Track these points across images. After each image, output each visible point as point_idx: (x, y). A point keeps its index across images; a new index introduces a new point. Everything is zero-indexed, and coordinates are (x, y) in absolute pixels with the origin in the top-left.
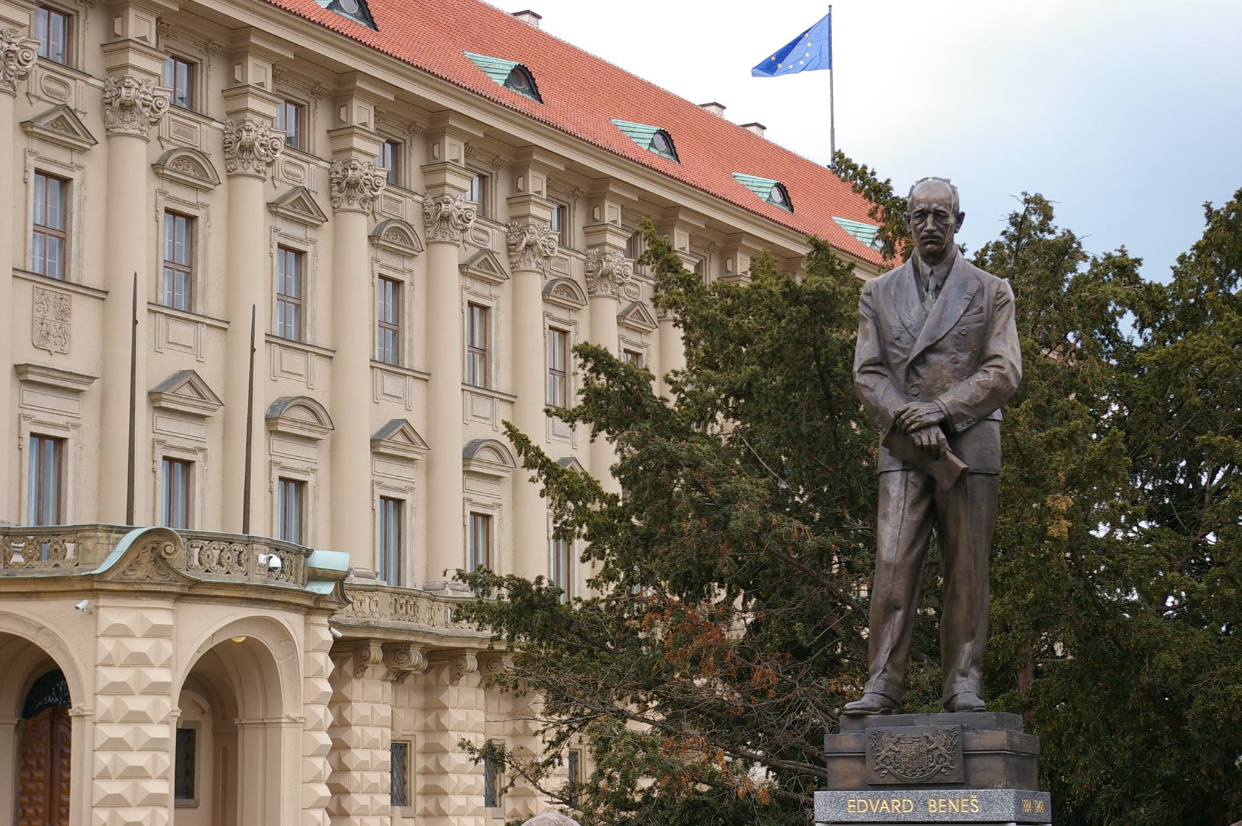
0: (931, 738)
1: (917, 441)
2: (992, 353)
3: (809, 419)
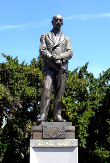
0: (59, 127)
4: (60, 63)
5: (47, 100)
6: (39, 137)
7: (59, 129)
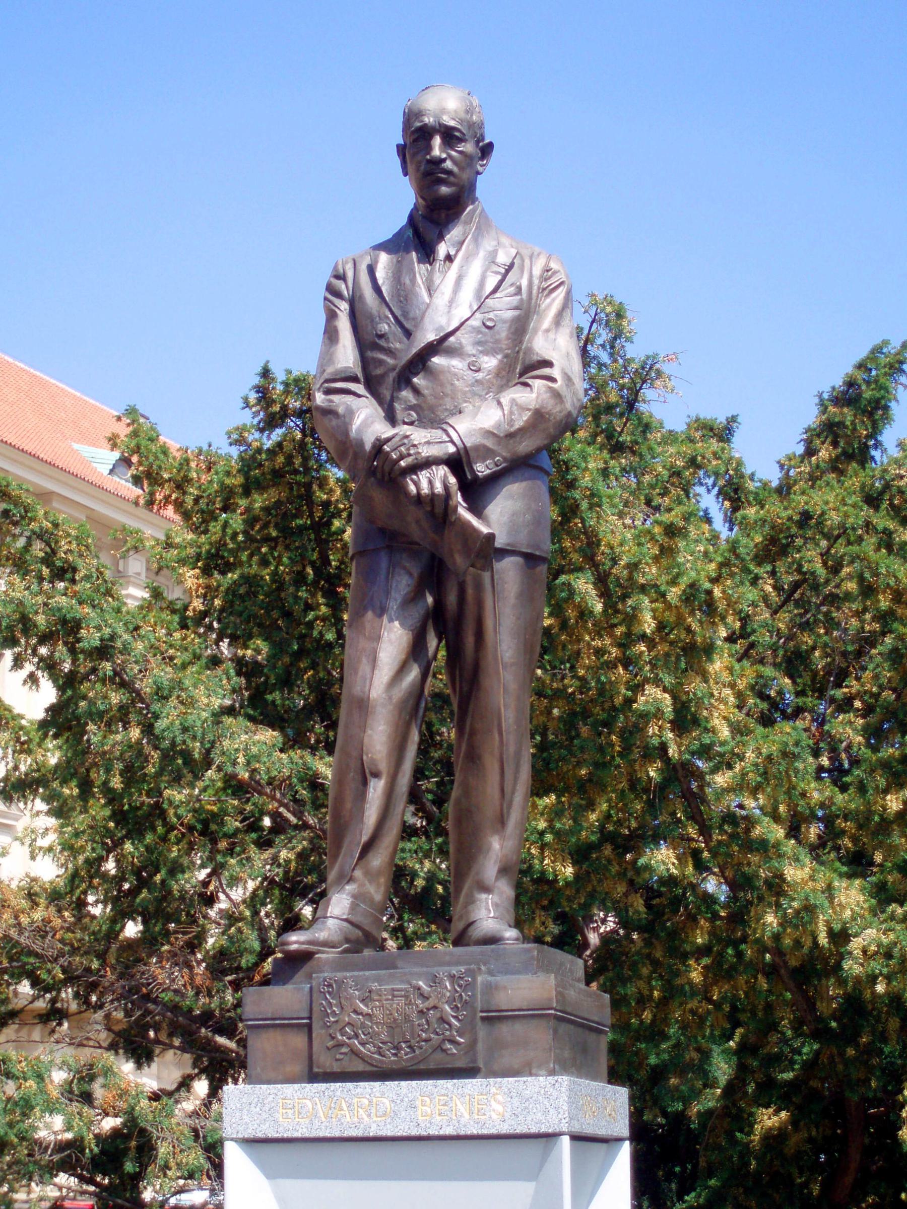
1: (412, 488)
3: (452, 977)
4: (439, 488)
5: (365, 783)
7: (427, 1004)
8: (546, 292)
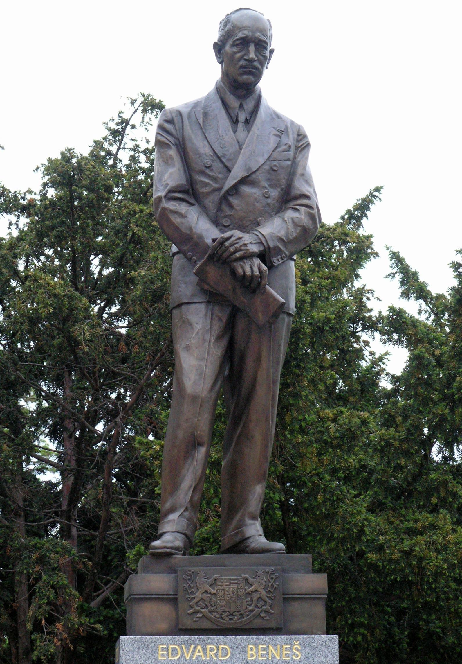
0: (251, 580)
1: (240, 271)
2: (297, 192)
4: (257, 273)
6: (164, 626)
7: (252, 589)
8: (300, 149)
